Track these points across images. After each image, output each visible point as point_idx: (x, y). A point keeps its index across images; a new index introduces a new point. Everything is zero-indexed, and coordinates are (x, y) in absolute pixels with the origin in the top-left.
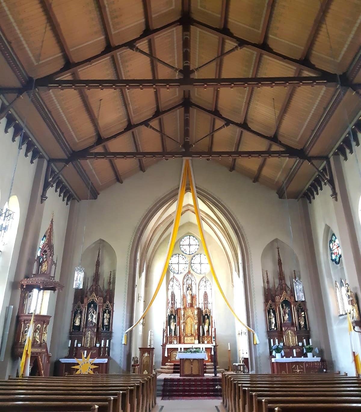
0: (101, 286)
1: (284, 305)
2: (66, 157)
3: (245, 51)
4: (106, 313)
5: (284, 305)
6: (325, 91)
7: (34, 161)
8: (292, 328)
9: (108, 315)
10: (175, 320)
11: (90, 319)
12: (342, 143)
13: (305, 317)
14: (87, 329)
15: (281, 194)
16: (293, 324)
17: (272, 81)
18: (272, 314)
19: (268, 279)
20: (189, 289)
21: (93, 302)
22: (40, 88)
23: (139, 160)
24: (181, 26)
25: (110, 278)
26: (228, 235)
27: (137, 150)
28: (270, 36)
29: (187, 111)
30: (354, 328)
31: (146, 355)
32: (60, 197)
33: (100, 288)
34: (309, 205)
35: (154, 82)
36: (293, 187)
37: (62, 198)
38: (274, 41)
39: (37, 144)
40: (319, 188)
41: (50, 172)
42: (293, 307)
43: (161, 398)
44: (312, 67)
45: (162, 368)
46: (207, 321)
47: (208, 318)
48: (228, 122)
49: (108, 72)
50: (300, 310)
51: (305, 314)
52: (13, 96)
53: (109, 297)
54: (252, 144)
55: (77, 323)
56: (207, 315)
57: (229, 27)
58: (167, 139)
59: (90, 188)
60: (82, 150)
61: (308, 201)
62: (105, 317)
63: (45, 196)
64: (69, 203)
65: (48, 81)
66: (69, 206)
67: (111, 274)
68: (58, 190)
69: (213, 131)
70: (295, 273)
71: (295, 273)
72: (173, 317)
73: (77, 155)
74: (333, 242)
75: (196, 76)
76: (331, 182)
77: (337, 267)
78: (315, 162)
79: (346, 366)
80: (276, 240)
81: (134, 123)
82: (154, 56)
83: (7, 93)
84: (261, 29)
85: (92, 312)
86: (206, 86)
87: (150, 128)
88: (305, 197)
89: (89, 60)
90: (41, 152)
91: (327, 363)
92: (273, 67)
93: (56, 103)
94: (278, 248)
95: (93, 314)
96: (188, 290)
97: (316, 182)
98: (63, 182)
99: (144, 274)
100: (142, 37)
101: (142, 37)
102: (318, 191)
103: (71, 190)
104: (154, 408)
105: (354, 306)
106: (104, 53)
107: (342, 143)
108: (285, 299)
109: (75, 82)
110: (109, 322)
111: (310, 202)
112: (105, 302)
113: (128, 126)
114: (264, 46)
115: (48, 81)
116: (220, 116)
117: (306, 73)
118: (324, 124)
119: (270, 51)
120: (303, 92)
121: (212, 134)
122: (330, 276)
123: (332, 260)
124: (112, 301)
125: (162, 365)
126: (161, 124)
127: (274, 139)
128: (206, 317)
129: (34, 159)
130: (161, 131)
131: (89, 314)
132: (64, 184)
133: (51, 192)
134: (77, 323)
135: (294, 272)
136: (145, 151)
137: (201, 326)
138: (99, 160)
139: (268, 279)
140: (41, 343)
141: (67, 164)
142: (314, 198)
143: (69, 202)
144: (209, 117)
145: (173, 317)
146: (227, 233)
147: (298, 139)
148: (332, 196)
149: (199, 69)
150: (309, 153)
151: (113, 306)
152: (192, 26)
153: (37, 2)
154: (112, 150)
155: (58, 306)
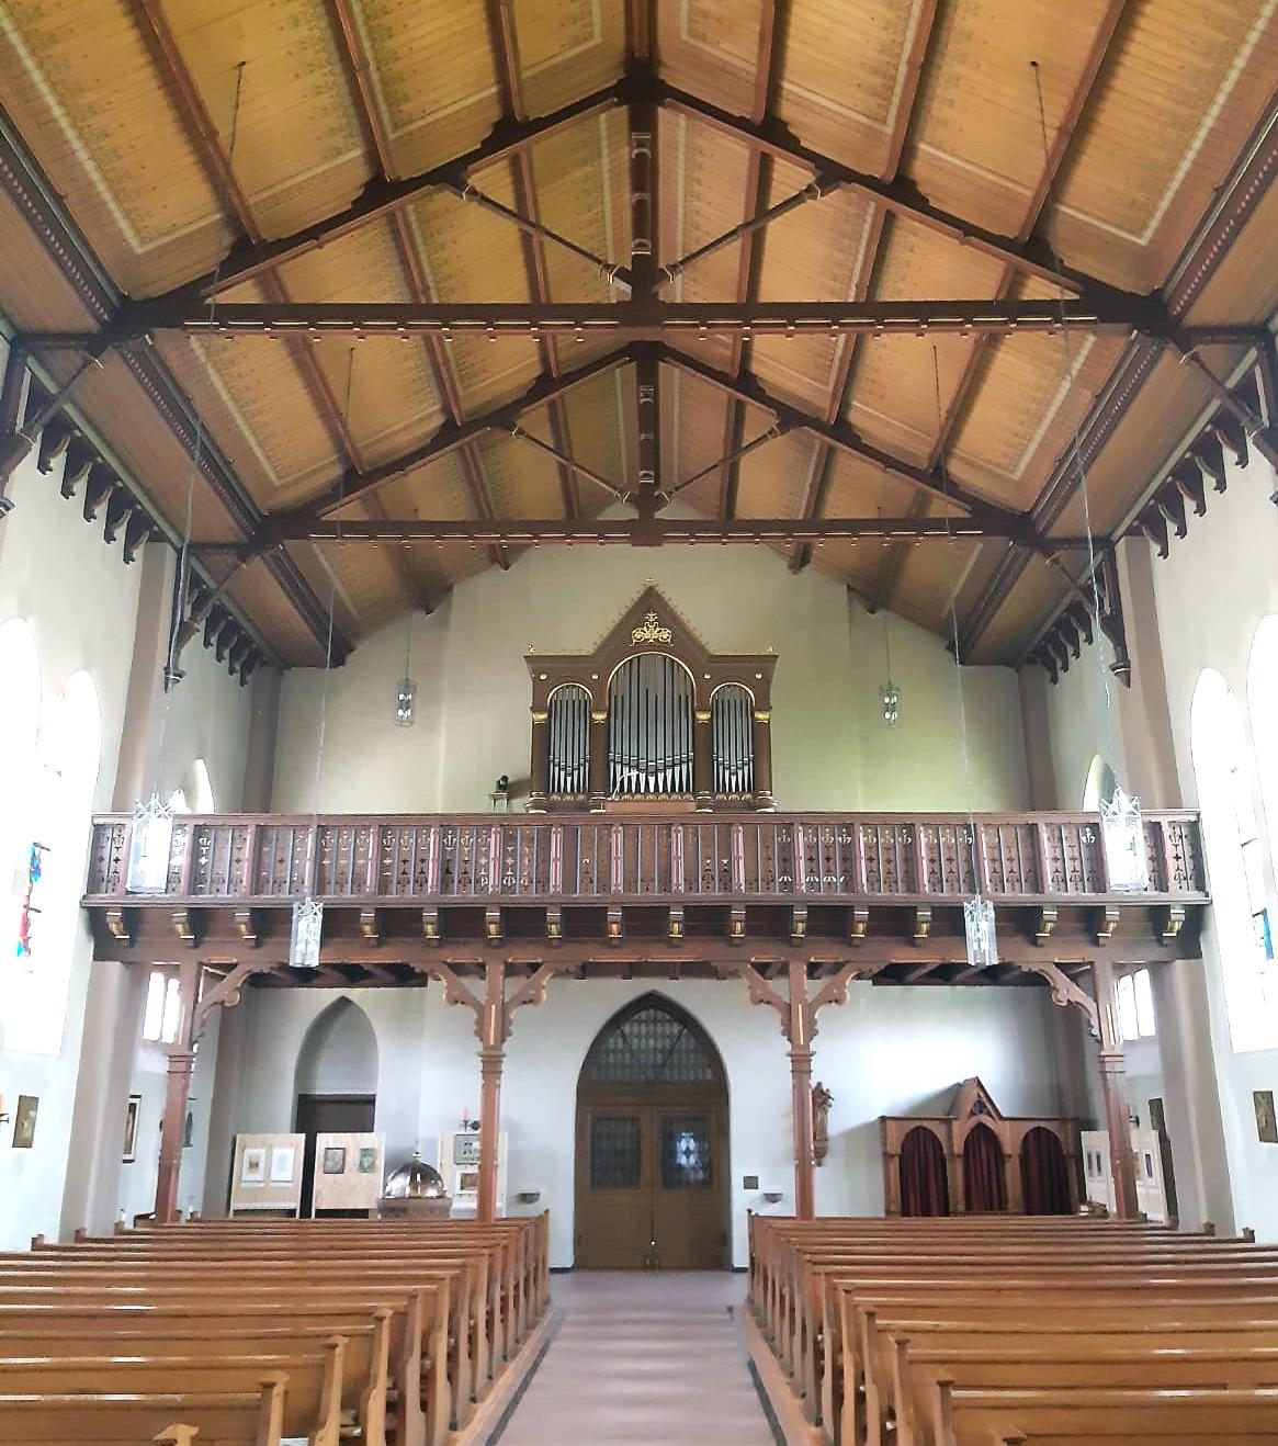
2: (89, 323)
3: (834, 202)
6: (1095, 343)
7: (53, 463)
12: (1170, 479)
17: (922, 314)
22: (158, 331)
23: (427, 339)
24: (625, 107)
27: (414, 293)
28: (854, 403)
29: (643, 123)
32: (219, 661)
34: (1049, 685)
35: (534, 311)
37: (100, 523)
38: (933, 164)
39: (123, 476)
40: (1172, 528)
44: (953, 489)
48: (830, 175)
49: (316, 78)
52: (69, 359)
54: (931, 266)
57: (787, 111)
58: (551, 247)
59: (197, 452)
60: (157, 299)
61: (1156, 548)
64: (137, 553)
65: (183, 305)
68: (101, 510)
69: (761, 212)
73: (276, 527)
75: (677, 290)
78: (1209, 352)
81: (399, 173)
83: (48, 348)
84: (891, 120)
87: (470, 201)
88: (1039, 660)
89: (316, 233)
90: (205, 583)
93: (64, 123)
97: (1180, 480)
98: (252, 642)
100: (490, 147)
101: (490, 147)
102: (1067, 657)
103: (246, 625)
104: (494, 1381)
106: (361, 206)
107: (1170, 479)
109: (269, 313)
113: (368, 186)
114: (901, 189)
115: (183, 305)
116: (792, 145)
117: (1038, 288)
118: (1189, 291)
119: (920, 204)
121: (731, 461)
127: (937, 475)
129: (53, 457)
130: (561, 448)
132: (255, 646)
136: (454, 299)
138: (349, 544)
141: (244, 561)
142: (1077, 654)
143: (99, 504)
144: (722, 393)
147: (1018, 475)
149: (682, 267)
150: (1186, 309)
152: (661, 110)
154: (299, 296)
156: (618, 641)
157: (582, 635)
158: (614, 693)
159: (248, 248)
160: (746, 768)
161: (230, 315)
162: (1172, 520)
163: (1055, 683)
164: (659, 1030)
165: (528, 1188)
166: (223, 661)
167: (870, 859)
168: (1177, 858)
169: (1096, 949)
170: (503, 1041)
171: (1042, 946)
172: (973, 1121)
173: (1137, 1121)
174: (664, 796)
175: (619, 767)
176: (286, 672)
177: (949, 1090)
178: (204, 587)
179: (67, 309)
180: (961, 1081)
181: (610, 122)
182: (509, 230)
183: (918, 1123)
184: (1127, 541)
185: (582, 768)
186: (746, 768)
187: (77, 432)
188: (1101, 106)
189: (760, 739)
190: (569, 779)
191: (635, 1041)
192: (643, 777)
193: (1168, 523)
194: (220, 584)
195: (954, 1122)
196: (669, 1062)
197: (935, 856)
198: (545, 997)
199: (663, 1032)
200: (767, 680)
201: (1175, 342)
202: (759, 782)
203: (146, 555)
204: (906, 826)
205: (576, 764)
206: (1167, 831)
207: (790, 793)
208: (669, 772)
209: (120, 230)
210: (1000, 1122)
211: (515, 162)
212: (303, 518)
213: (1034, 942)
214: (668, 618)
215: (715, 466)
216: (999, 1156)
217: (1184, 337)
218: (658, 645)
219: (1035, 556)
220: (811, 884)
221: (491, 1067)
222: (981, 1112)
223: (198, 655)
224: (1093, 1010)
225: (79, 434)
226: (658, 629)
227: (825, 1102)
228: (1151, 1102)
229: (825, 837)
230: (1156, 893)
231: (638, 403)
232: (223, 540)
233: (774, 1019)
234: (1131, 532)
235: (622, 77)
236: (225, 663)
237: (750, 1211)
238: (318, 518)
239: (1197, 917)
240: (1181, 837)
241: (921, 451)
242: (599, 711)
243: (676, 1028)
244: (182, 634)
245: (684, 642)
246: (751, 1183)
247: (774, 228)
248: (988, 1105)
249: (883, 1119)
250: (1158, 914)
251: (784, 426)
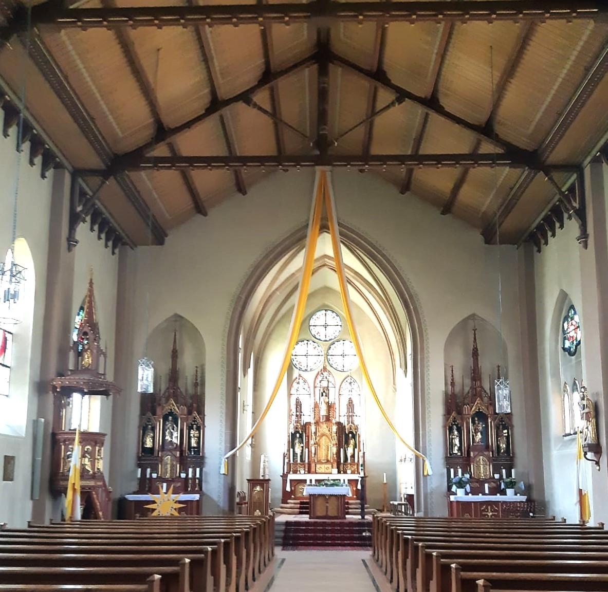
0: (183, 390)
1: (476, 419)
2: (103, 167)
4: (193, 429)
5: (476, 419)
8: (486, 453)
9: (197, 432)
10: (303, 440)
11: (168, 438)
13: (508, 437)
14: (165, 453)
15: (489, 236)
16: (487, 448)
18: (456, 433)
19: (453, 380)
20: (324, 394)
21: (171, 414)
25: (196, 376)
26: (391, 309)
29: (323, 72)
30: (585, 454)
31: (258, 488)
33: (181, 392)
34: (536, 255)
36: (510, 223)
41: (78, 195)
42: (491, 422)
43: (281, 548)
45: (282, 508)
46: (352, 442)
47: (354, 437)
48: (402, 95)
50: (501, 427)
51: (508, 433)
53: (196, 405)
55: (149, 444)
56: (352, 433)
62: (192, 435)
63: (74, 238)
64: (47, 174)
66: (117, 256)
67: (197, 371)
68: (96, 227)
69: (373, 112)
70: (499, 370)
71: (499, 370)
72: (298, 435)
73: (122, 162)
74: (570, 320)
77: (571, 361)
78: (556, 175)
79: (564, 507)
80: (473, 317)
85: (171, 428)
89: (188, 125)
91: (536, 504)
94: (475, 330)
95: (172, 431)
96: (322, 395)
99: (251, 371)
105: (590, 422)
108: (479, 409)
109: (175, 160)
110: (198, 443)
111: (539, 251)
112: (190, 413)
116: (387, 83)
117: (487, 148)
121: (370, 120)
122: (556, 375)
123: (564, 349)
124: (201, 412)
125: (282, 503)
127: (486, 130)
128: (350, 435)
129: (47, 171)
131: (166, 430)
133: (83, 230)
134: (149, 444)
135: (497, 368)
137: (342, 450)
139: (453, 380)
140: (94, 473)
142: (546, 243)
144: (365, 83)
145: (298, 435)
146: (390, 306)
148: (578, 240)
151: (203, 420)
152: (331, 64)
155: (115, 417)
159: (162, 132)
161: (157, 162)
162: (558, 222)
166: (108, 248)
178: (117, 233)
179: (93, 161)
181: (308, 73)
182: (267, 121)
184: (591, 166)
187: (7, 97)
188: (501, 103)
193: (548, 232)
201: (543, 171)
203: (120, 251)
209: (80, 69)
211: (272, 90)
212: (135, 158)
215: (362, 123)
217: (548, 170)
225: (48, 147)
231: (314, 485)
235: (316, 51)
241: (480, 118)
244: (74, 219)
247: (379, 120)
251: (400, 100)
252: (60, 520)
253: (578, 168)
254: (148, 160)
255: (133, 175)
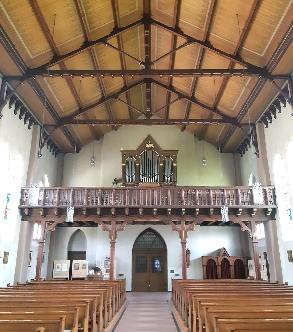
2: (20, 74)
3: (191, 46)
6: (251, 79)
7: (12, 106)
12: (268, 110)
17: (211, 72)
22: (36, 76)
23: (98, 78)
24: (143, 25)
27: (95, 67)
28: (196, 93)
29: (147, 28)
32: (50, 152)
34: (240, 157)
35: (123, 71)
37: (23, 120)
38: (214, 38)
39: (28, 109)
40: (269, 121)
41: (45, 136)
44: (219, 112)
48: (190, 40)
52: (16, 82)
54: (213, 61)
57: (180, 25)
58: (126, 57)
59: (45, 104)
60: (36, 69)
61: (265, 126)
64: (31, 127)
65: (42, 70)
68: (23, 117)
69: (174, 49)
73: (63, 121)
75: (155, 66)
76: (256, 144)
78: (277, 81)
81: (91, 40)
82: (122, 50)
83: (11, 80)
84: (204, 28)
86: (161, 76)
87: (108, 46)
88: (238, 151)
89: (72, 54)
90: (47, 134)
92: (213, 61)
93: (15, 28)
97: (271, 110)
100: (112, 34)
101: (112, 34)
102: (245, 151)
103: (56, 143)
106: (83, 47)
107: (268, 110)
109: (62, 72)
113: (84, 43)
114: (207, 43)
115: (42, 70)
116: (182, 33)
117: (238, 66)
118: (273, 67)
119: (211, 47)
120: (234, 83)
121: (168, 106)
126: (128, 97)
127: (215, 109)
129: (12, 105)
130: (129, 103)
132: (58, 148)
138: (80, 125)
141: (56, 129)
142: (247, 150)
143: (23, 116)
144: (166, 90)
147: (233, 109)
148: (255, 154)
149: (156, 61)
150: (272, 71)
152: (151, 25)
153: (27, 2)
154: (69, 68)
156: (142, 147)
157: (133, 146)
158: (141, 159)
159: (57, 57)
160: (171, 176)
161: (53, 72)
162: (269, 119)
163: (242, 157)
164: (151, 236)
165: (121, 273)
166: (51, 152)
167: (200, 197)
168: (270, 197)
169: (251, 218)
170: (115, 239)
171: (239, 217)
172: (223, 257)
173: (261, 257)
174: (152, 183)
175: (142, 176)
176: (66, 154)
177: (218, 250)
178: (47, 135)
179: (15, 71)
180: (220, 248)
181: (140, 28)
182: (117, 53)
183: (210, 258)
184: (258, 124)
185: (133, 176)
186: (171, 176)
187: (18, 99)
188: (253, 24)
189: (174, 170)
190: (130, 179)
191: (146, 239)
192: (147, 178)
193: (268, 120)
194: (50, 134)
195: (219, 258)
196: (153, 244)
197: (214, 197)
198: (125, 229)
199: (152, 237)
200: (176, 156)
202: (174, 179)
203: (33, 127)
204: (208, 190)
205: (132, 175)
206: (267, 191)
207: (181, 182)
208: (153, 177)
209: (28, 53)
210: (229, 258)
211: (118, 37)
212: (69, 119)
213: (237, 216)
214: (153, 142)
215: (164, 107)
216: (229, 265)
217: (271, 77)
218: (151, 148)
219: (237, 128)
220: (186, 203)
221: (113, 245)
222: (225, 255)
223: (45, 150)
224: (251, 232)
225: (18, 100)
226: (151, 144)
227: (189, 253)
228: (264, 253)
229: (189, 192)
230: (265, 205)
232: (51, 124)
233: (177, 234)
234: (259, 122)
235: (143, 18)
236: (52, 152)
237: (172, 278)
238: (73, 119)
239: (274, 210)
240: (271, 192)
242: (137, 163)
243: (155, 236)
244: (42, 145)
245: (157, 147)
246: (172, 272)
247: (178, 52)
248: (226, 254)
249: (202, 257)
250: (266, 210)
251: (180, 98)
252: (26, 283)
253: (253, 125)
254: (75, 121)
255: (67, 125)
